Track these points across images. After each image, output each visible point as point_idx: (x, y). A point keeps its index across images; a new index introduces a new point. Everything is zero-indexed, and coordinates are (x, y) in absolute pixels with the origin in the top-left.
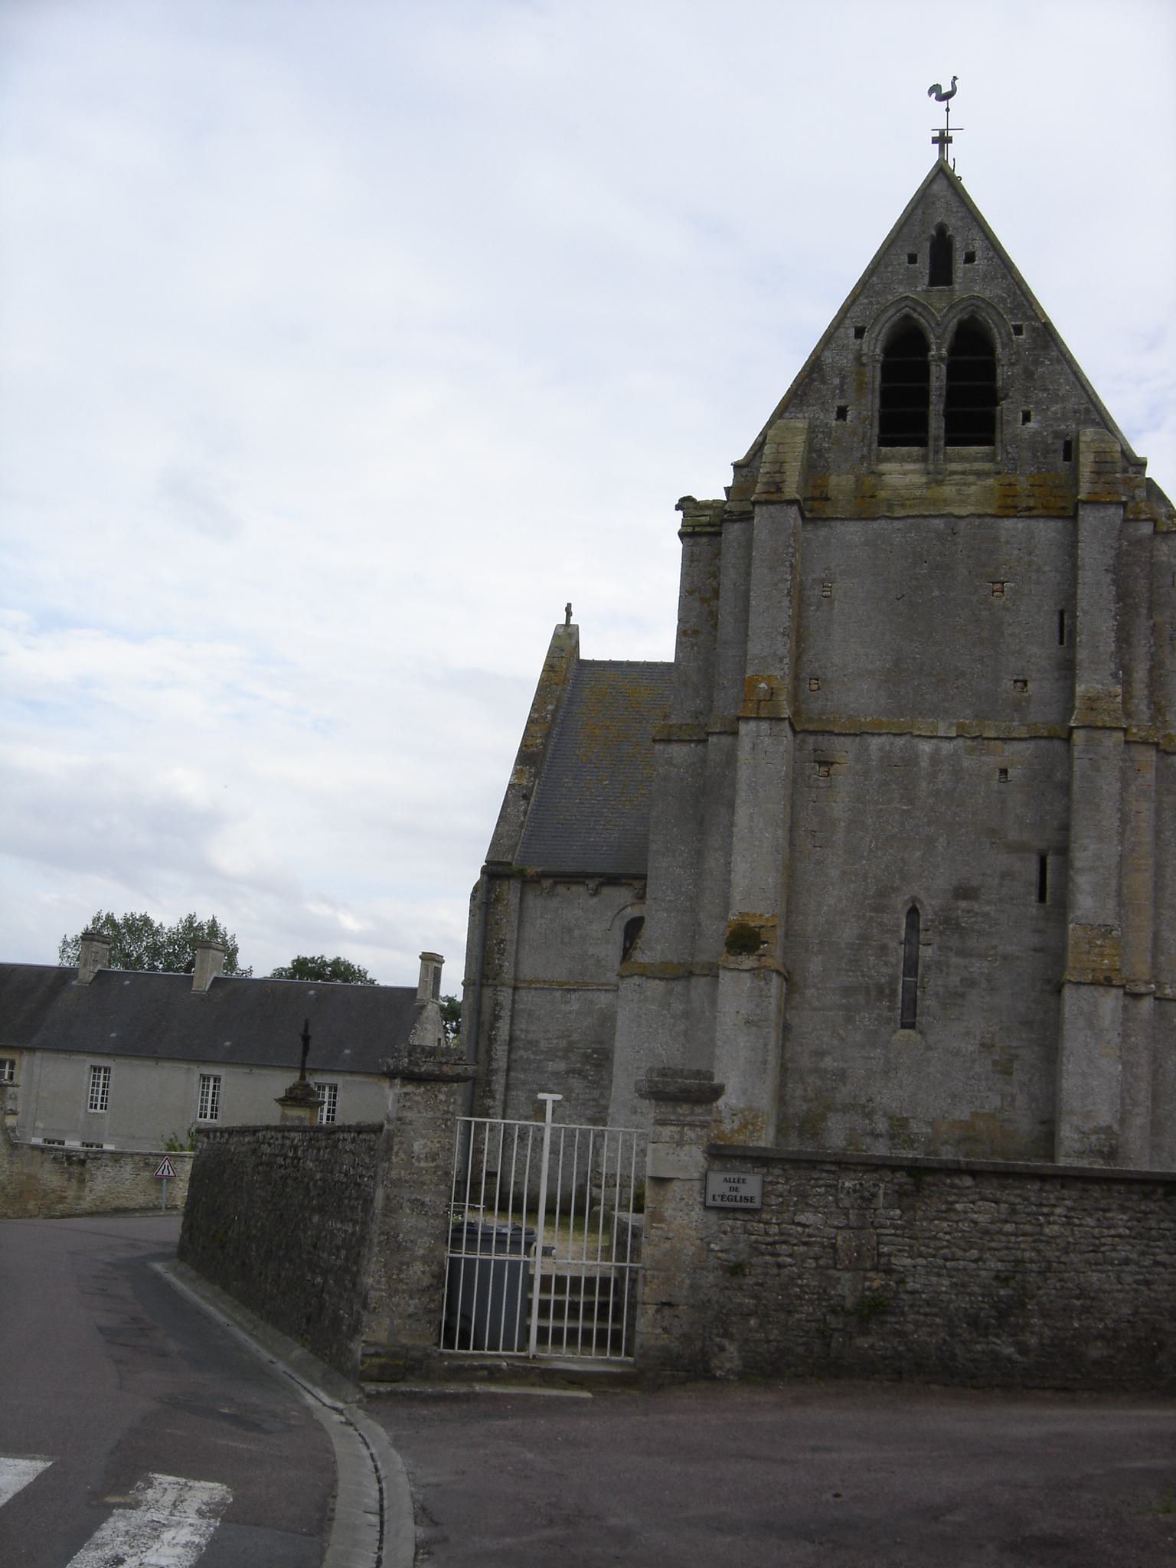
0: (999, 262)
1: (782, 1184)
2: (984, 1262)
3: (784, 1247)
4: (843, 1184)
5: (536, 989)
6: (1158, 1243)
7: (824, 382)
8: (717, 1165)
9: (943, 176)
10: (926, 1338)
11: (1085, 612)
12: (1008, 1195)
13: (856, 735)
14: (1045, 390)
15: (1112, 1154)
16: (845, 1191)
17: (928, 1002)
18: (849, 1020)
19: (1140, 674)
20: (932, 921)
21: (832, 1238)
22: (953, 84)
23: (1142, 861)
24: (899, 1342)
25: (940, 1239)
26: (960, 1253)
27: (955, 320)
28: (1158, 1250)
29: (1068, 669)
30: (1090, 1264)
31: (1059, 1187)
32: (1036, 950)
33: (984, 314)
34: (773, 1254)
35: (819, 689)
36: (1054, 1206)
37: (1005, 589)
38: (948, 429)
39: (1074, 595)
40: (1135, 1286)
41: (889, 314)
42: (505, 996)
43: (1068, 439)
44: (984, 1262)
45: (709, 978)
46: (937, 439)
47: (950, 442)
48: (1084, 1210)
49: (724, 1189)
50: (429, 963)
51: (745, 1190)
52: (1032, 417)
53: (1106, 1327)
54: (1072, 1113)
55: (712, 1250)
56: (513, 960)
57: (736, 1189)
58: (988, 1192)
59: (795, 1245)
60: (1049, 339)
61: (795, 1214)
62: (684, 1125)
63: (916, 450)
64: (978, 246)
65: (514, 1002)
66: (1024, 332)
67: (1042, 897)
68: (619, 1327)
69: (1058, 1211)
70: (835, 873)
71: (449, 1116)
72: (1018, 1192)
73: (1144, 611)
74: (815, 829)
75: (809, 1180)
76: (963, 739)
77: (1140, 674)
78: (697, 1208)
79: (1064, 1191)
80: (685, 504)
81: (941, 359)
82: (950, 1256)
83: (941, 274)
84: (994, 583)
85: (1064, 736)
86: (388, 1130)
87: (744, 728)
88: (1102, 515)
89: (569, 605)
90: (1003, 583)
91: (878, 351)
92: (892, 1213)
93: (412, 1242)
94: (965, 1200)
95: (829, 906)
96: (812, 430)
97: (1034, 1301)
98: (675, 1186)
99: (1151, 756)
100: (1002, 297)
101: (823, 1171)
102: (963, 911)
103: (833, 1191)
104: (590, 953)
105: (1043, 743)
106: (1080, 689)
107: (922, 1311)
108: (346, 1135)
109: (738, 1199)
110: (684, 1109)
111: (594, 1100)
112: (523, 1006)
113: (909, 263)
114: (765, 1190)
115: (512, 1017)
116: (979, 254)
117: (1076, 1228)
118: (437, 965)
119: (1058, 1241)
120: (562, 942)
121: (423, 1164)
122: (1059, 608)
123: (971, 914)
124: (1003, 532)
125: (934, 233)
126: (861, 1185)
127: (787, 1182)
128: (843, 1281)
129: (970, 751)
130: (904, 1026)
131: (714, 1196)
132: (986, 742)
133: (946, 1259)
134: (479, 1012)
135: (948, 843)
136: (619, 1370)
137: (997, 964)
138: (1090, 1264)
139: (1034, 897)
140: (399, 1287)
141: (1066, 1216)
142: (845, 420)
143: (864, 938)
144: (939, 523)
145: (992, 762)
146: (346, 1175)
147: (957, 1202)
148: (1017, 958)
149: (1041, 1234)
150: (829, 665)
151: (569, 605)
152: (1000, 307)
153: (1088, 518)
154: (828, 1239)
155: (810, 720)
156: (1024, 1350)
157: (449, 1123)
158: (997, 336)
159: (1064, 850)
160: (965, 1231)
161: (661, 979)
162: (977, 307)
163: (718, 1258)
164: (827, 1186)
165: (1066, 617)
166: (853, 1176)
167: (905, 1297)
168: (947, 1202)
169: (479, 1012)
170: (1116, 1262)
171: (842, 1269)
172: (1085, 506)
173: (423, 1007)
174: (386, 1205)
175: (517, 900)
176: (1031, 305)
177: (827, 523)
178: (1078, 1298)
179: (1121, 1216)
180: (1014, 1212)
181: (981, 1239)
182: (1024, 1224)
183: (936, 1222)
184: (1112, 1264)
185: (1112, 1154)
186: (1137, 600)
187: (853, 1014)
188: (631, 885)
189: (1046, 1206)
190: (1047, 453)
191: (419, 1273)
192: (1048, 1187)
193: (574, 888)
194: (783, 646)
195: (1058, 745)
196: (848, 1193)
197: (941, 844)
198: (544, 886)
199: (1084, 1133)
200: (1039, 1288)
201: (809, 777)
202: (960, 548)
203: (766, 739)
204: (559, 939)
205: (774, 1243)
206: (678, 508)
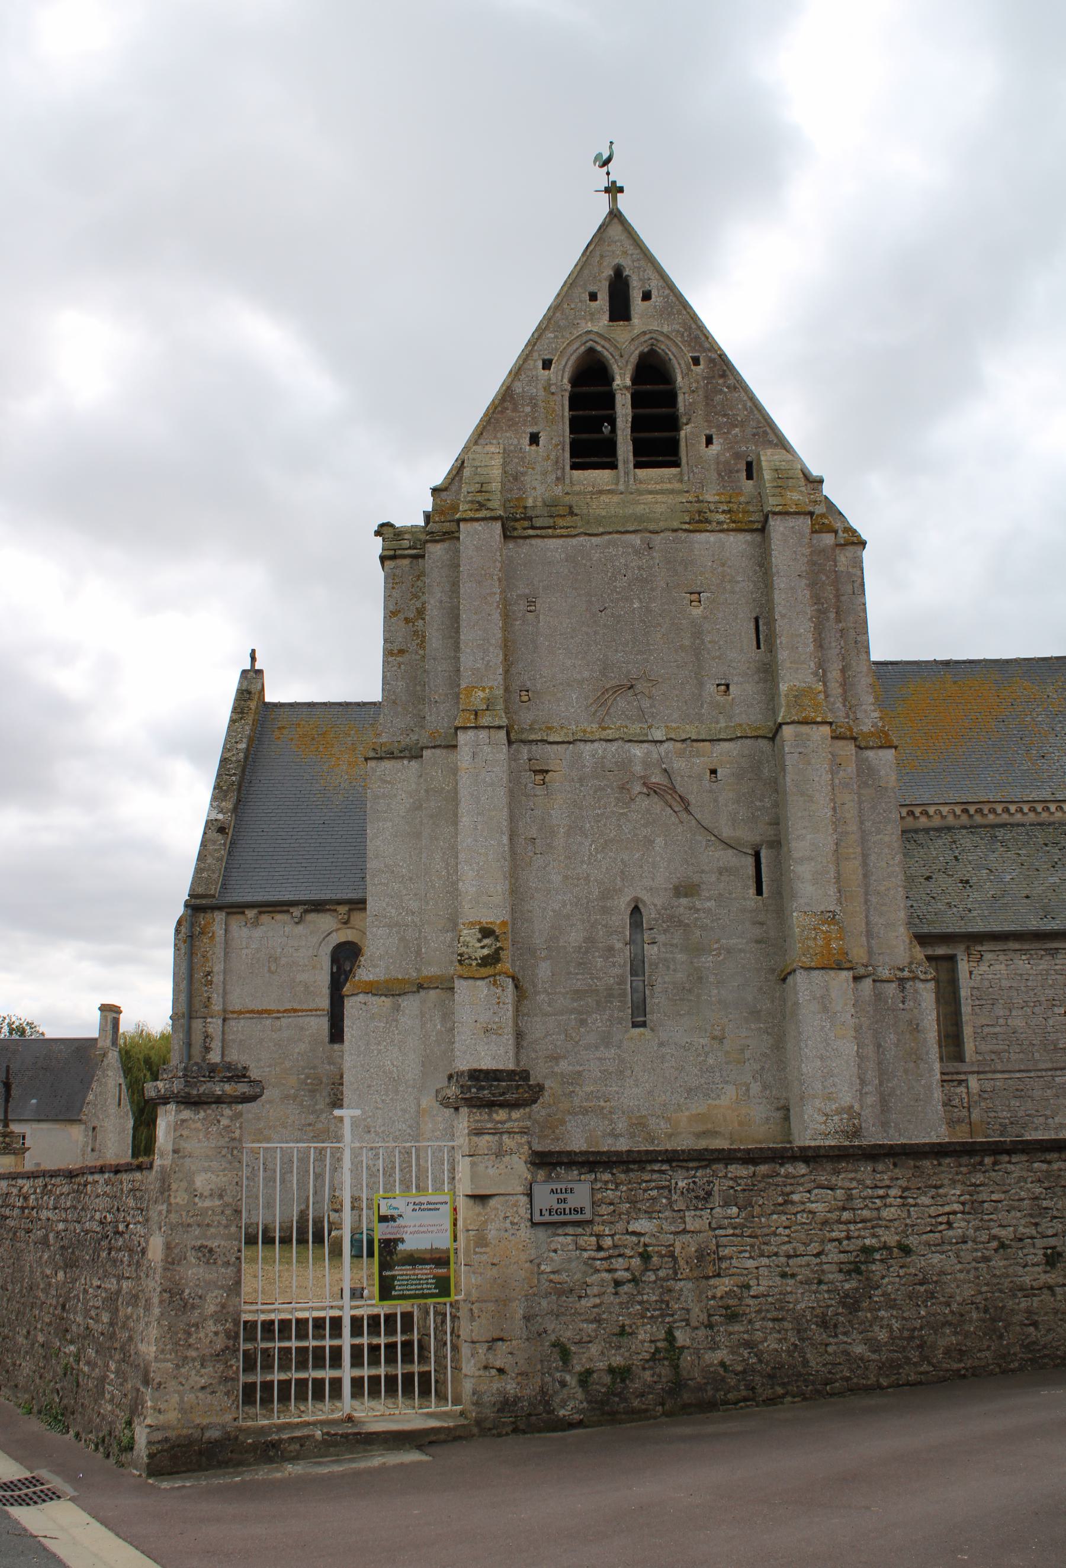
0: (674, 299)
1: (612, 1190)
2: (827, 1255)
3: (620, 1260)
4: (676, 1183)
5: (244, 1018)
6: (991, 1216)
7: (515, 410)
8: (541, 1174)
9: (615, 215)
10: (776, 1346)
11: (783, 616)
12: (843, 1179)
13: (569, 743)
14: (725, 415)
15: (857, 1133)
16: (678, 1191)
17: (657, 1000)
18: (583, 1022)
19: (834, 674)
20: (655, 919)
21: (670, 1246)
22: (610, 147)
23: (851, 850)
24: (749, 1353)
25: (780, 1235)
26: (801, 1249)
27: (637, 352)
28: (992, 1223)
29: (768, 672)
30: (929, 1245)
31: (891, 1167)
32: (758, 942)
33: (663, 347)
34: (609, 1271)
35: (529, 700)
36: (889, 1187)
37: (702, 599)
38: (636, 453)
39: (770, 601)
40: (974, 1264)
41: (575, 347)
42: (215, 1026)
43: (749, 459)
44: (827, 1255)
45: (438, 990)
46: (626, 462)
47: (638, 465)
48: (919, 1189)
49: (552, 1201)
50: (107, 1013)
51: (573, 1201)
52: (714, 440)
53: (952, 1312)
54: (814, 1097)
55: (543, 1273)
56: (221, 991)
57: (565, 1201)
58: (822, 1179)
59: (631, 1257)
60: (725, 368)
61: (628, 1223)
62: (502, 1133)
63: (674, 471)
64: (654, 285)
65: (223, 1033)
66: (702, 362)
67: (759, 892)
68: (426, 1369)
69: (893, 1192)
70: (556, 879)
71: (235, 1144)
72: (852, 1175)
73: (832, 615)
74: (534, 836)
75: (640, 1184)
76: (673, 742)
77: (834, 674)
78: (525, 1225)
79: (897, 1171)
80: (385, 530)
81: (626, 388)
82: (791, 1252)
83: (620, 310)
84: (691, 593)
85: (771, 736)
86: (162, 1166)
87: (463, 737)
88: (791, 525)
89: (253, 651)
90: (699, 593)
91: (566, 381)
92: (729, 1211)
93: (200, 1297)
94: (801, 1189)
95: (554, 911)
96: (506, 454)
97: (879, 1292)
98: (493, 1202)
99: (851, 750)
100: (678, 331)
101: (654, 1171)
102: (685, 908)
103: (666, 1192)
104: (298, 980)
105: (748, 742)
106: (783, 687)
107: (769, 1316)
108: (97, 1177)
109: (567, 1211)
110: (501, 1115)
111: (310, 1125)
112: (233, 1037)
113: (590, 300)
114: (596, 1199)
115: (223, 1048)
116: (654, 293)
117: (912, 1209)
118: (115, 1015)
119: (896, 1223)
120: (270, 971)
121: (208, 1203)
122: (754, 615)
123: (692, 911)
124: (696, 545)
125: (611, 273)
126: (694, 1182)
127: (616, 1189)
128: (685, 1292)
129: (680, 754)
130: (635, 1025)
131: (541, 1210)
132: (695, 744)
133: (789, 1257)
134: (189, 1045)
135: (666, 844)
136: (451, 1424)
137: (721, 958)
138: (929, 1245)
139: (752, 891)
140: (188, 1354)
141: (901, 1197)
142: (538, 445)
143: (590, 940)
144: (636, 540)
145: (701, 763)
146: (101, 1223)
147: (792, 1193)
148: (741, 951)
149: (879, 1219)
150: (538, 676)
151: (253, 651)
152: (678, 340)
153: (778, 527)
154: (667, 1246)
155: (522, 731)
156: (875, 1346)
157: (235, 1152)
158: (677, 366)
159: (777, 844)
160: (804, 1223)
161: (386, 996)
162: (657, 340)
163: (551, 1281)
164: (658, 1188)
165: (761, 623)
166: (686, 1174)
167: (751, 1302)
168: (783, 1194)
169: (189, 1045)
170: (954, 1241)
171: (684, 1279)
172: (776, 517)
173: (104, 1055)
174: (167, 1256)
175: (222, 932)
176: (707, 338)
177: (528, 541)
178: (921, 1284)
179: (953, 1192)
180: (850, 1198)
181: (821, 1230)
182: (862, 1209)
183: (775, 1216)
184: (951, 1243)
185: (857, 1133)
186: (825, 606)
187: (585, 1016)
188: (335, 910)
189: (881, 1188)
190: (731, 472)
191: (211, 1334)
192: (880, 1167)
193: (279, 917)
194: (496, 657)
195: (763, 744)
196: (682, 1193)
197: (659, 841)
198: (249, 916)
199: (826, 1115)
200: (883, 1277)
201: (526, 786)
202: (657, 561)
203: (485, 747)
204: (266, 969)
205: (610, 1257)
206: (378, 533)
